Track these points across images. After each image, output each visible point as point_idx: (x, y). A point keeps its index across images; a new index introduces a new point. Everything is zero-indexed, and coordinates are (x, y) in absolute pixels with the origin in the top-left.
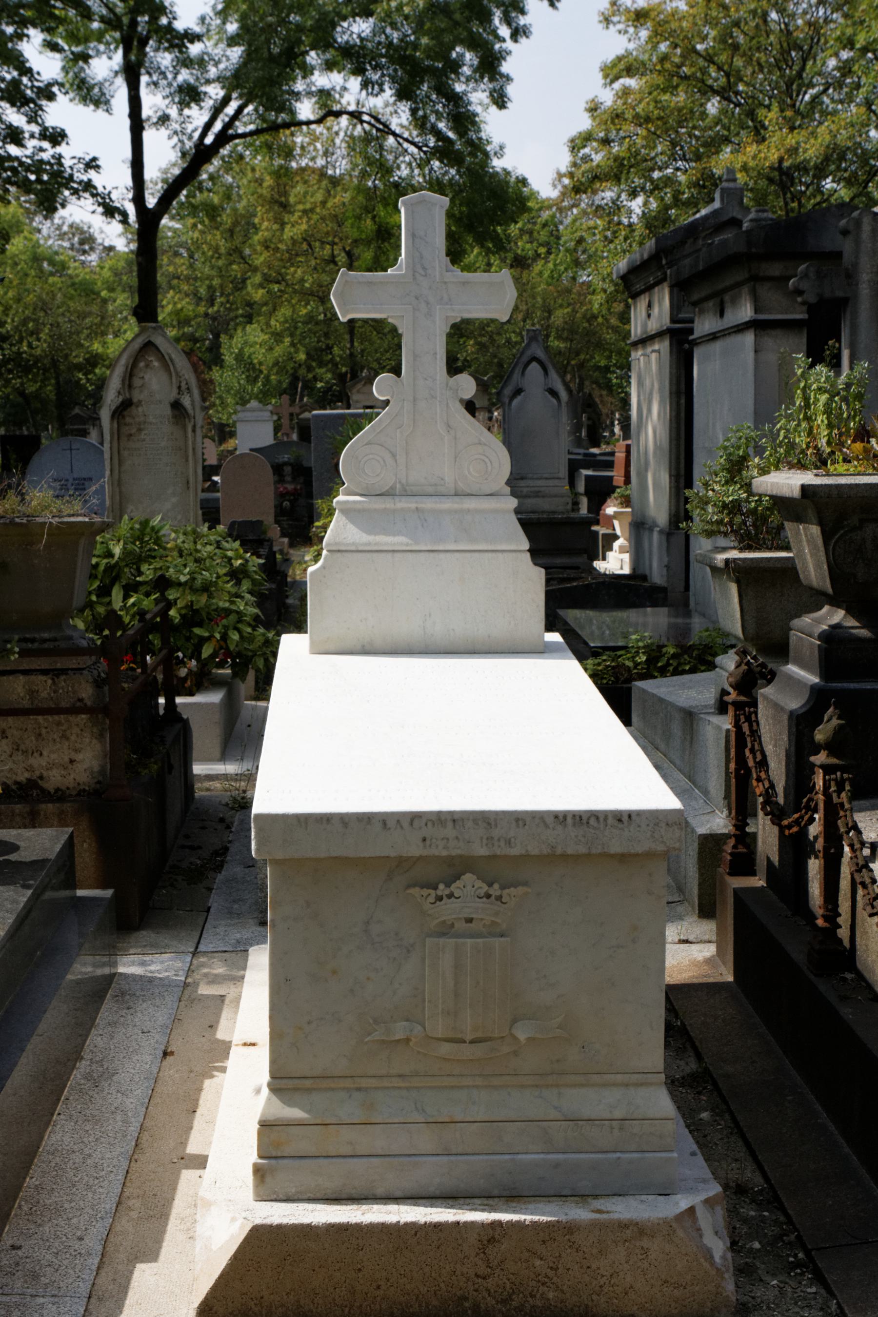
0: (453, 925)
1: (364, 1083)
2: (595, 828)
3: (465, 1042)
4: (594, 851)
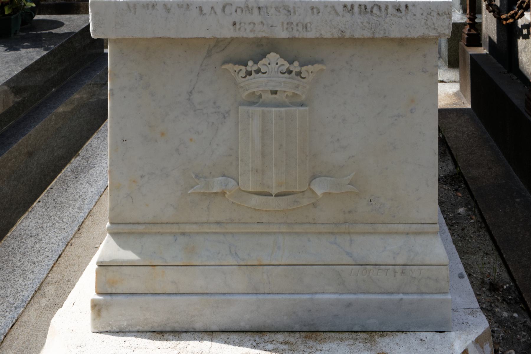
0: (260, 96)
1: (188, 228)
2: (378, 16)
3: (271, 195)
4: (377, 36)
